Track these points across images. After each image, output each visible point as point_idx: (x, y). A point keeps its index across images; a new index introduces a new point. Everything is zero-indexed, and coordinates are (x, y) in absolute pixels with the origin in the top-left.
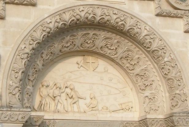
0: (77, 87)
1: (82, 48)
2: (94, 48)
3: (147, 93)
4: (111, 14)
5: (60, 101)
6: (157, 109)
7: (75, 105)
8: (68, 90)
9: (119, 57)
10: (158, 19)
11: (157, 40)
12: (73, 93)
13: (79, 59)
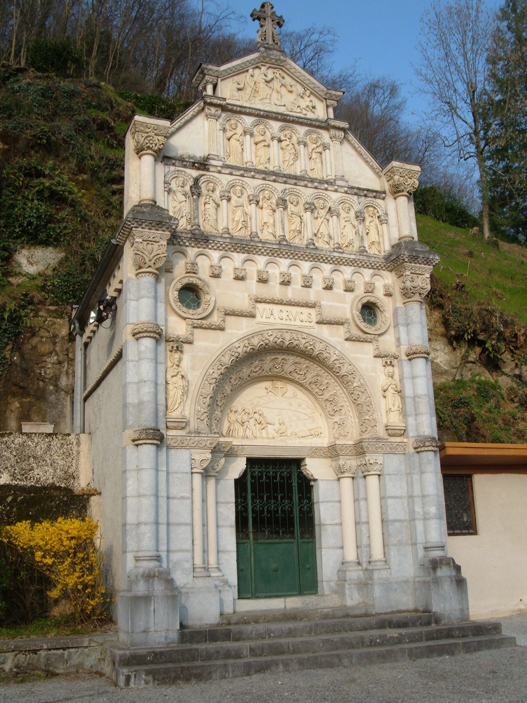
3: (337, 418)
4: (300, 339)
8: (257, 416)
9: (308, 383)
10: (347, 344)
11: (346, 365)
12: (261, 419)
13: (268, 384)
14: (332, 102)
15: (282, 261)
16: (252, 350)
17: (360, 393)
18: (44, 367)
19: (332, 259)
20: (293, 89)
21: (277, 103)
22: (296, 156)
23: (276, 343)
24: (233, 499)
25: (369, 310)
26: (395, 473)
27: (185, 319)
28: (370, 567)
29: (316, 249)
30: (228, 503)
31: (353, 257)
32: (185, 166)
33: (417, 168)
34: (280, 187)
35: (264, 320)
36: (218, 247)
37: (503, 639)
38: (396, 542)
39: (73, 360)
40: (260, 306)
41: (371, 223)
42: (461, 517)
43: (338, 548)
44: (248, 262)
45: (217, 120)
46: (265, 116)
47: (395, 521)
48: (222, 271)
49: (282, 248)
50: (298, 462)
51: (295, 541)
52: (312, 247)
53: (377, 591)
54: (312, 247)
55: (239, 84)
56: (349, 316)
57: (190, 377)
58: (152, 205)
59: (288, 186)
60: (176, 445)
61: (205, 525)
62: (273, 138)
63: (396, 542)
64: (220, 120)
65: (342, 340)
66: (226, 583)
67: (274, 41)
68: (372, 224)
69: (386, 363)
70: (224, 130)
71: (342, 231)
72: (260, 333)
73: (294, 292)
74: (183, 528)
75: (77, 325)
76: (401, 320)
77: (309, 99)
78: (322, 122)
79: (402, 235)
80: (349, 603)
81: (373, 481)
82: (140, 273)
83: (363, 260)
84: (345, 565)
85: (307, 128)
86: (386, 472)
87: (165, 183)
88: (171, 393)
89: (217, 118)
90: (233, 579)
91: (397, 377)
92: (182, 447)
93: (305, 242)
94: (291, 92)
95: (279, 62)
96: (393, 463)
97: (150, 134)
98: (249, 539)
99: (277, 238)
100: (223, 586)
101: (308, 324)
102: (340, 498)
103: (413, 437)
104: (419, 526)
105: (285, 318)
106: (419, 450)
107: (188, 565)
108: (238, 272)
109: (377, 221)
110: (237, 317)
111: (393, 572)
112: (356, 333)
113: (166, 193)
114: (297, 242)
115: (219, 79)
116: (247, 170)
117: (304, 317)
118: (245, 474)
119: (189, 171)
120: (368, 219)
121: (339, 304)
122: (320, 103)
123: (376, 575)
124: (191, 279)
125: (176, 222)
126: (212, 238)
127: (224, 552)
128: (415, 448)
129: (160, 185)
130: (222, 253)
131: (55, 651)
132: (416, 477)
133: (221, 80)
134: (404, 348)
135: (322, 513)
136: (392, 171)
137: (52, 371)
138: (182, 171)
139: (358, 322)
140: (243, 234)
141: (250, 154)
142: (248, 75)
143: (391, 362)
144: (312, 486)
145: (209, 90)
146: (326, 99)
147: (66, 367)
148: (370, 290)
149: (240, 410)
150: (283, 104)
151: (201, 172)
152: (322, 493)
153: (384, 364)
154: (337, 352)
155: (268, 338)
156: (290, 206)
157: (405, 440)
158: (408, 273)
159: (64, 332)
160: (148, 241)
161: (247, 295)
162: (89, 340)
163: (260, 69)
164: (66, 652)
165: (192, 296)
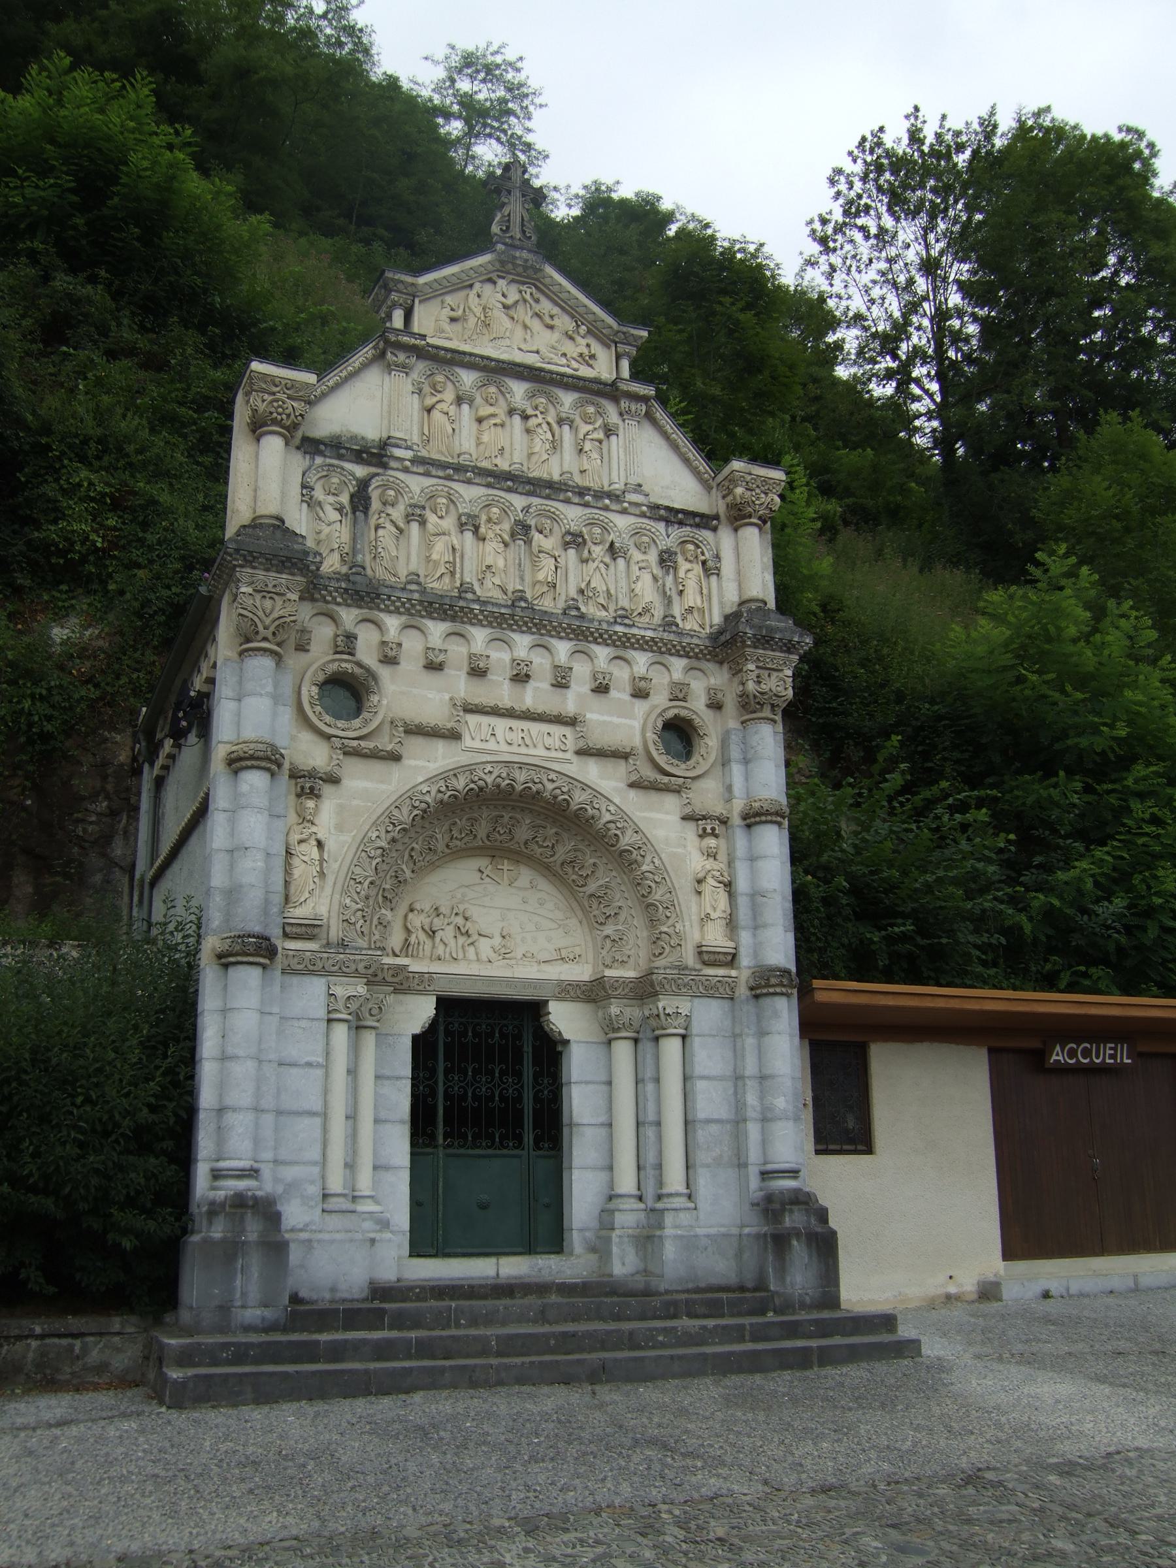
0: (473, 911)
3: (609, 930)
9: (559, 863)
10: (632, 794)
11: (629, 832)
13: (483, 862)
14: (628, 348)
15: (516, 637)
16: (452, 799)
17: (653, 885)
18: (83, 821)
19: (610, 636)
21: (523, 347)
22: (555, 445)
23: (555, 797)
24: (408, 1072)
25: (679, 733)
26: (714, 1033)
27: (328, 737)
28: (659, 1205)
29: (582, 617)
30: (398, 1078)
31: (650, 634)
32: (340, 457)
34: (518, 501)
35: (477, 744)
37: (899, 1342)
38: (710, 1160)
39: (137, 809)
40: (473, 719)
42: (842, 1124)
43: (386, 1121)
44: (658, 666)
45: (407, 374)
46: (498, 371)
47: (708, 1121)
49: (516, 615)
50: (534, 1010)
51: (525, 1153)
52: (574, 613)
53: (670, 1251)
54: (574, 613)
55: (452, 310)
56: (637, 741)
57: (331, 845)
58: (274, 525)
59: (536, 501)
62: (511, 412)
63: (710, 1160)
64: (415, 375)
65: (622, 785)
66: (385, 1224)
67: (524, 232)
68: (690, 575)
69: (704, 829)
71: (633, 586)
72: (470, 769)
73: (535, 696)
74: (307, 1121)
75: (144, 744)
76: (735, 753)
77: (583, 342)
78: (606, 384)
79: (745, 597)
81: (671, 1048)
82: (247, 650)
83: (667, 643)
84: (614, 1201)
85: (576, 395)
86: (694, 1031)
87: (303, 486)
88: (297, 873)
89: (405, 369)
90: (402, 1218)
91: (723, 856)
92: (312, 973)
93: (561, 604)
94: (551, 327)
95: (530, 272)
96: (707, 1015)
97: (279, 396)
99: (510, 594)
100: (380, 1231)
101: (560, 755)
102: (611, 1076)
103: (749, 968)
104: (753, 1130)
105: (515, 742)
106: (758, 992)
107: (314, 1190)
108: (431, 655)
109: (698, 568)
110: (428, 739)
111: (702, 1216)
112: (649, 774)
114: (547, 604)
115: (417, 301)
116: (459, 468)
118: (434, 1023)
119: (348, 466)
120: (683, 566)
121: (623, 721)
122: (605, 349)
123: (669, 1219)
124: (344, 665)
125: (318, 559)
126: (386, 591)
128: (752, 989)
129: (295, 490)
130: (404, 618)
131: (56, 1340)
132: (750, 1042)
134: (738, 805)
135: (576, 1102)
136: (732, 480)
137: (97, 828)
139: (655, 754)
140: (441, 585)
141: (466, 438)
142: (472, 294)
143: (713, 829)
144: (561, 1053)
145: (398, 320)
146: (616, 343)
147: (124, 821)
148: (681, 696)
149: (427, 906)
150: (535, 348)
151: (373, 470)
152: (580, 1064)
153: (701, 832)
154: (612, 808)
155: (484, 776)
156: (537, 536)
157: (734, 973)
158: (751, 666)
159: (123, 757)
160: (263, 592)
161: (447, 697)
162: (163, 773)
163: (495, 283)
164: (78, 1344)
165: (342, 694)
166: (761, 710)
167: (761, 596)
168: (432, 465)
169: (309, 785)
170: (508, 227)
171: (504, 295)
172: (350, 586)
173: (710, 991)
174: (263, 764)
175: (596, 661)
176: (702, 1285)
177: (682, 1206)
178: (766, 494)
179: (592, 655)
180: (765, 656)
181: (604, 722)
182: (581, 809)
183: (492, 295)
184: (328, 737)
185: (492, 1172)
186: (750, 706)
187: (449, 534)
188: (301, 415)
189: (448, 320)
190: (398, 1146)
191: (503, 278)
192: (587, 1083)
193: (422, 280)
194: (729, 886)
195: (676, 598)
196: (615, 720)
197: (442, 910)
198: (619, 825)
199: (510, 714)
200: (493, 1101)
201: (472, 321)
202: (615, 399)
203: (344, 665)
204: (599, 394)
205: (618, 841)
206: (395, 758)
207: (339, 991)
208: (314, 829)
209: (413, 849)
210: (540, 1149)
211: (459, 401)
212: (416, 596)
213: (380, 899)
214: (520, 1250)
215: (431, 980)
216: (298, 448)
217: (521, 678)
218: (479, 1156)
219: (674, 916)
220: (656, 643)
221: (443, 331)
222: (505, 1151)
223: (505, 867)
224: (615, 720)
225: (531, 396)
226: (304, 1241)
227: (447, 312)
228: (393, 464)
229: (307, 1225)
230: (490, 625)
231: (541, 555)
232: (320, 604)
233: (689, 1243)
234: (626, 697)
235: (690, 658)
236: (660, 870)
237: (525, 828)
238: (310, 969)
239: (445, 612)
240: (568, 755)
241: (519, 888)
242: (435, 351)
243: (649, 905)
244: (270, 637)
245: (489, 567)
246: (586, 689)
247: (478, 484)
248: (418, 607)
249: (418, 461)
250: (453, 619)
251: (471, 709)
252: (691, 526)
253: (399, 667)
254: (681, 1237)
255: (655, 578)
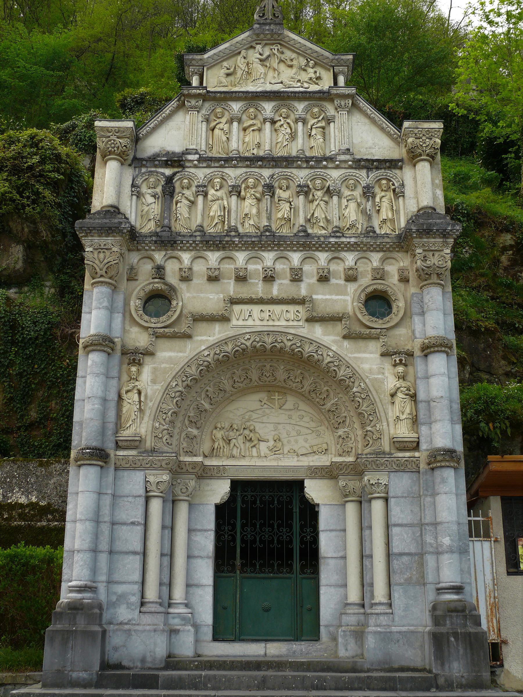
0: (258, 427)
1: (262, 383)
2: (277, 381)
3: (341, 432)
4: (285, 341)
5: (236, 444)
6: (350, 450)
7: (254, 450)
8: (247, 432)
9: (307, 391)
10: (346, 343)
11: (343, 368)
12: (252, 435)
13: (263, 396)
14: (341, 68)
15: (265, 254)
16: (225, 358)
17: (360, 400)
20: (295, 62)
21: (273, 82)
22: (293, 136)
24: (69, 526)
25: (378, 302)
26: (405, 495)
27: (147, 328)
31: (353, 240)
32: (156, 166)
33: (438, 125)
34: (266, 173)
35: (241, 323)
36: (188, 247)
40: (237, 308)
41: (384, 199)
44: (226, 260)
45: (198, 112)
46: (254, 98)
47: (401, 554)
48: (192, 274)
49: (267, 240)
53: (371, 642)
55: (228, 69)
59: (277, 170)
60: (128, 465)
61: (365, 556)
64: (203, 112)
70: (207, 121)
77: (312, 71)
79: (420, 207)
80: (342, 653)
81: (378, 506)
87: (133, 186)
88: (124, 410)
92: (135, 469)
94: (291, 66)
96: (400, 484)
98: (235, 573)
100: (184, 625)
101: (295, 323)
103: (427, 450)
104: (430, 561)
107: (135, 599)
111: (396, 619)
113: (134, 197)
114: (285, 231)
115: (205, 69)
117: (291, 316)
120: (379, 194)
123: (372, 621)
127: (197, 586)
133: (208, 69)
138: (154, 172)
139: (360, 316)
146: (333, 67)
148: (378, 277)
149: (227, 425)
150: (280, 81)
151: (176, 170)
152: (325, 519)
165: (159, 302)
166: (429, 278)
167: (431, 204)
168: (211, 161)
169: (135, 357)
170: (264, 14)
171: (260, 54)
172: (158, 239)
173: (401, 468)
174: (99, 348)
175: (319, 262)
176: (396, 666)
177: (382, 611)
178: (431, 139)
179: (317, 259)
180: (428, 242)
181: (326, 299)
182: (311, 355)
183: (254, 56)
184: (147, 328)
185: (266, 590)
186: (426, 276)
187: (222, 199)
188: (125, 146)
189: (225, 76)
190: (205, 572)
191: (260, 44)
192: (331, 531)
193: (206, 56)
194: (414, 397)
195: (374, 215)
196: (334, 297)
197: (235, 426)
198: (335, 364)
199: (261, 301)
200: (273, 544)
201: (239, 73)
202: (332, 100)
203: (155, 285)
204: (320, 99)
205: (336, 374)
206: (188, 336)
207: (151, 479)
208: (137, 383)
209: (207, 391)
210: (304, 573)
211: (231, 121)
212: (198, 238)
213: (187, 422)
214: (291, 638)
215: (224, 469)
216: (130, 165)
217: (269, 278)
218: (264, 578)
219: (375, 419)
220: (359, 245)
221: (221, 83)
222: (281, 575)
223: (277, 397)
224: (334, 297)
225: (276, 110)
226: (126, 631)
227: (224, 71)
228: (187, 164)
229: (130, 621)
230: (247, 249)
231: (280, 202)
232: (143, 252)
233: (386, 637)
234: (342, 282)
235: (384, 251)
236: (366, 391)
237: (281, 372)
238: (134, 467)
239: (217, 246)
240: (301, 323)
241: (286, 410)
242: (214, 95)
243: (360, 413)
244: (104, 274)
245: (246, 215)
246: (314, 280)
247: (241, 167)
248: (200, 245)
249: (201, 159)
250: (224, 248)
251: (234, 301)
252: (385, 169)
253: (193, 282)
254: (380, 633)
255: (359, 205)
